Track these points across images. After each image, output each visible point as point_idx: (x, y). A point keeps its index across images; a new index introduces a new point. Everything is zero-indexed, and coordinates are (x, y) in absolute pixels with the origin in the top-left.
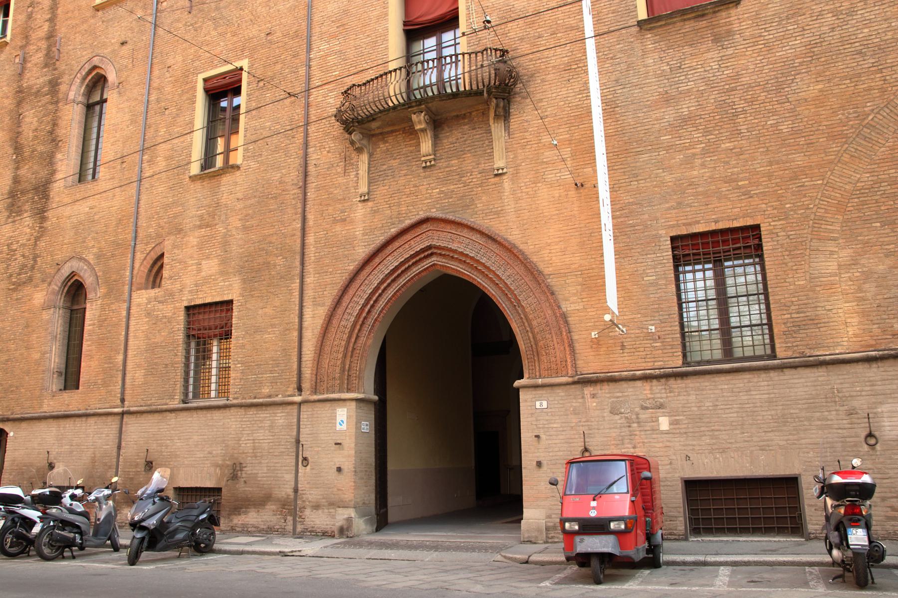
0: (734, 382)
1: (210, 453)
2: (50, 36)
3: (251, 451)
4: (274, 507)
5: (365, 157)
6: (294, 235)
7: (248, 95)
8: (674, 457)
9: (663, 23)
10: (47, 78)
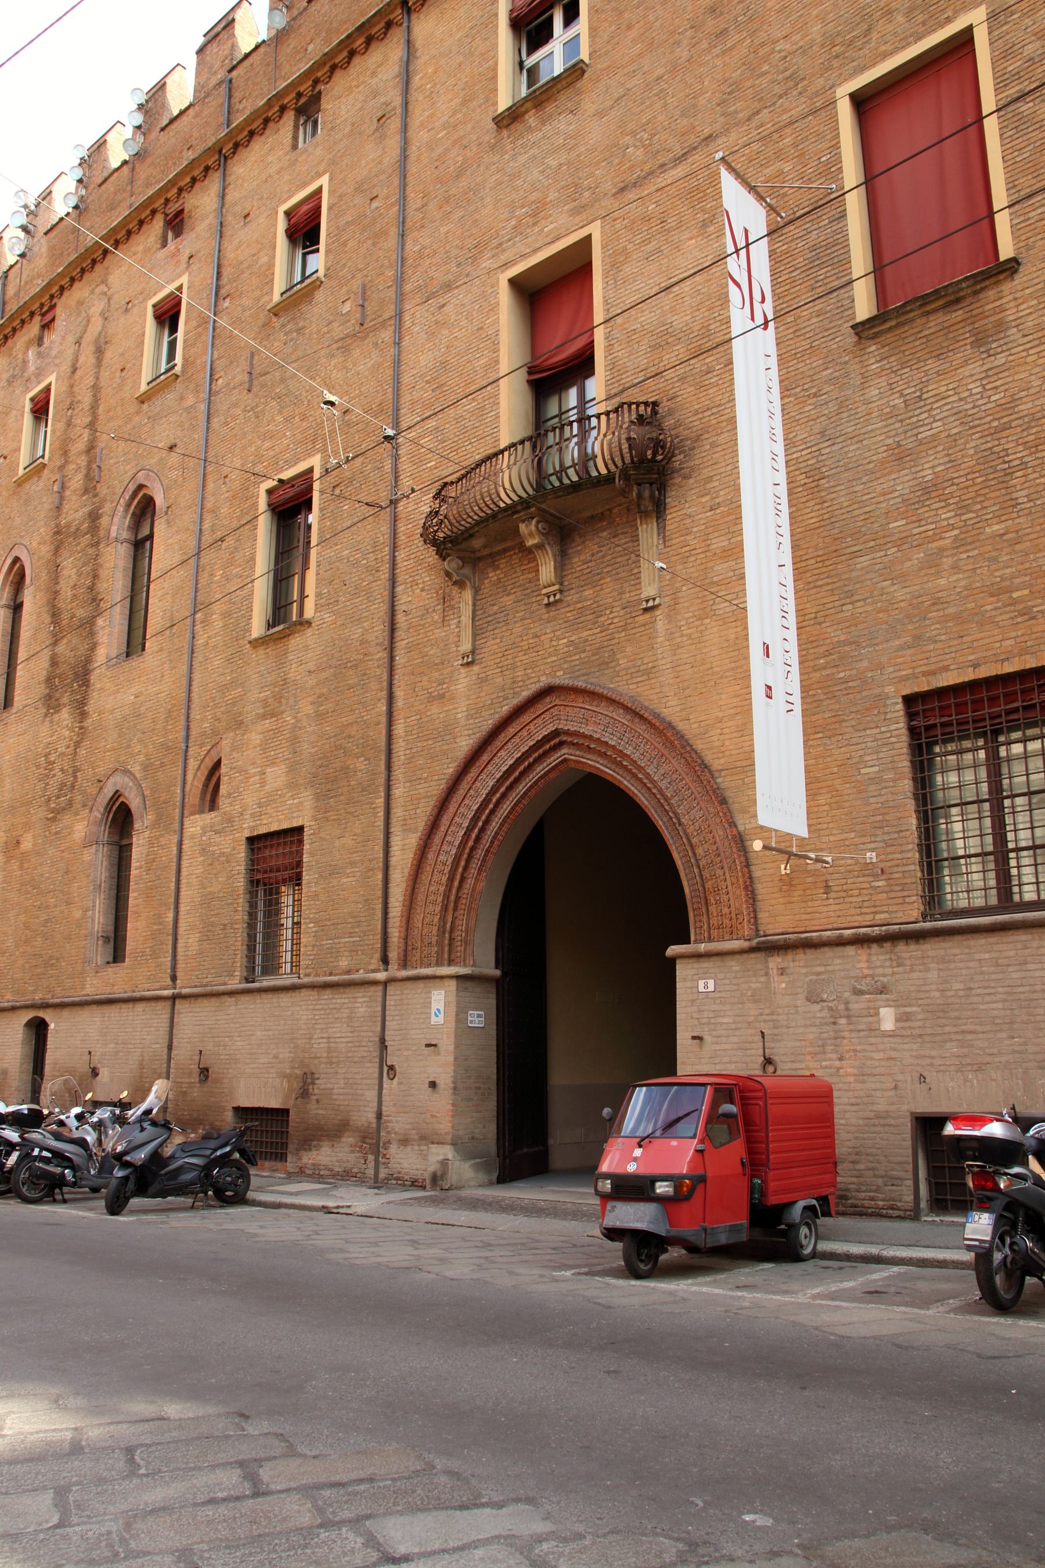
0: (1000, 947)
1: (276, 1057)
2: (91, 448)
3: (325, 1055)
4: (351, 1140)
5: (468, 595)
6: (379, 723)
7: (321, 510)
8: (900, 1077)
9: (893, 323)
10: (86, 510)
